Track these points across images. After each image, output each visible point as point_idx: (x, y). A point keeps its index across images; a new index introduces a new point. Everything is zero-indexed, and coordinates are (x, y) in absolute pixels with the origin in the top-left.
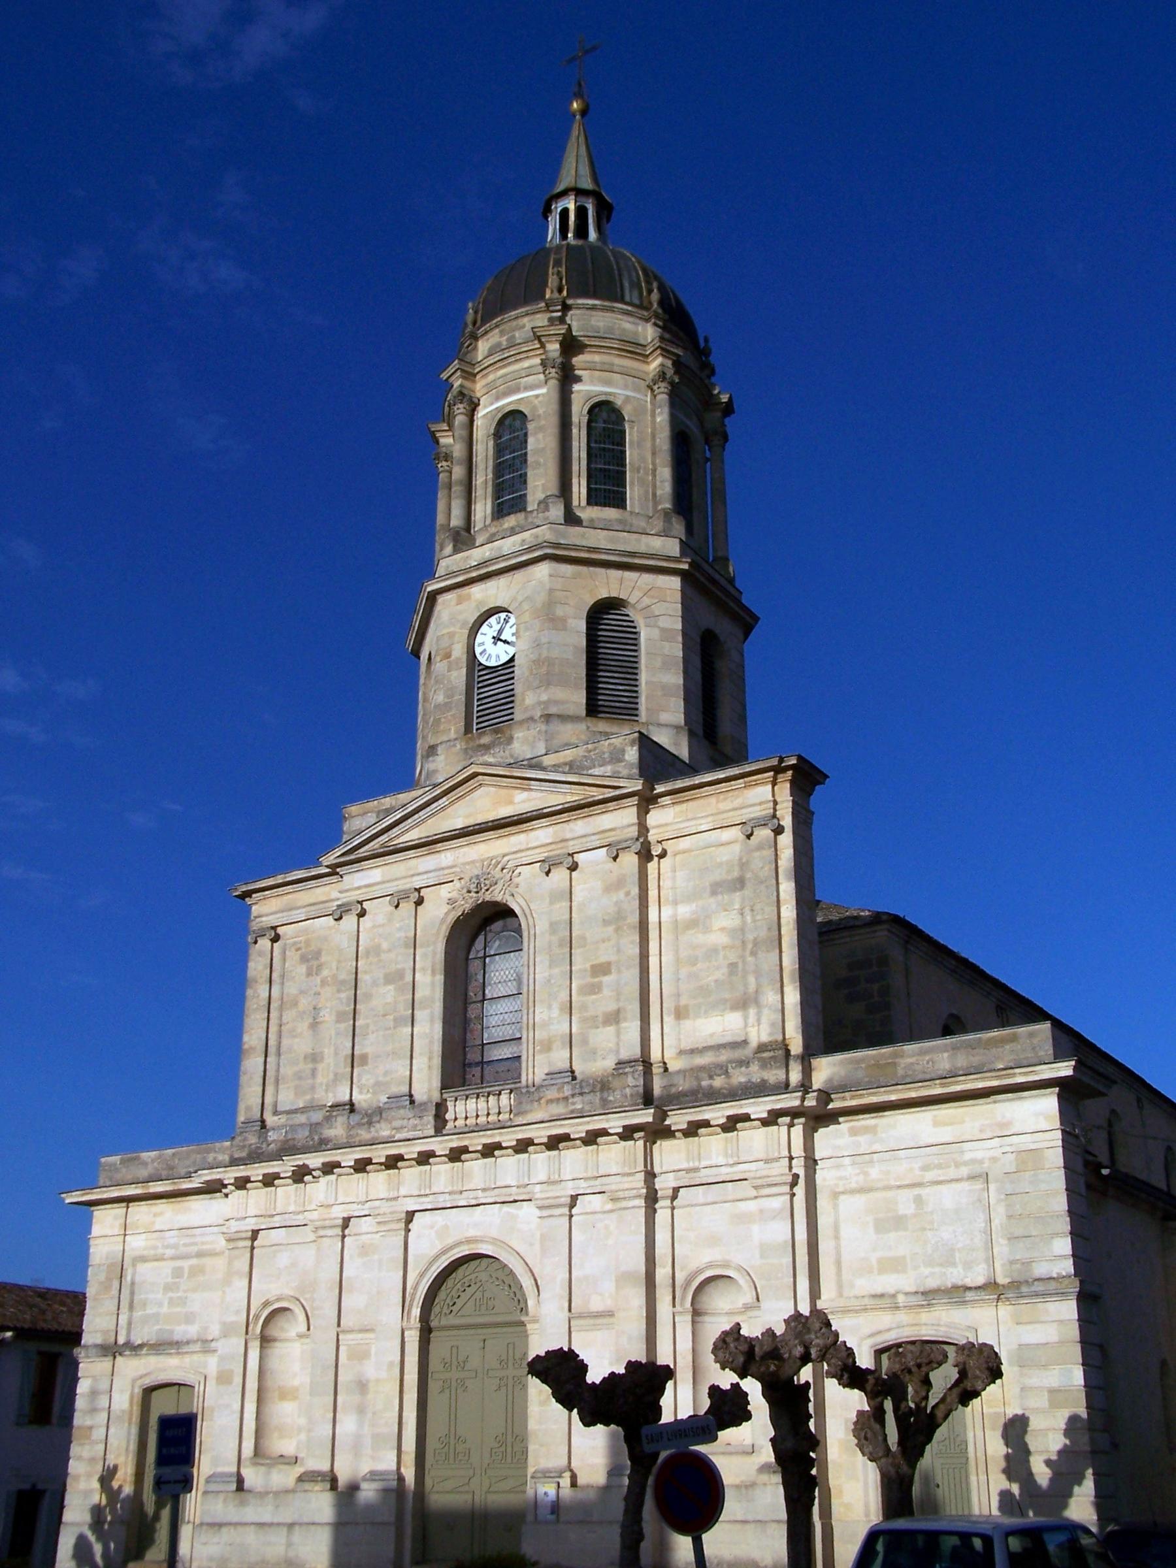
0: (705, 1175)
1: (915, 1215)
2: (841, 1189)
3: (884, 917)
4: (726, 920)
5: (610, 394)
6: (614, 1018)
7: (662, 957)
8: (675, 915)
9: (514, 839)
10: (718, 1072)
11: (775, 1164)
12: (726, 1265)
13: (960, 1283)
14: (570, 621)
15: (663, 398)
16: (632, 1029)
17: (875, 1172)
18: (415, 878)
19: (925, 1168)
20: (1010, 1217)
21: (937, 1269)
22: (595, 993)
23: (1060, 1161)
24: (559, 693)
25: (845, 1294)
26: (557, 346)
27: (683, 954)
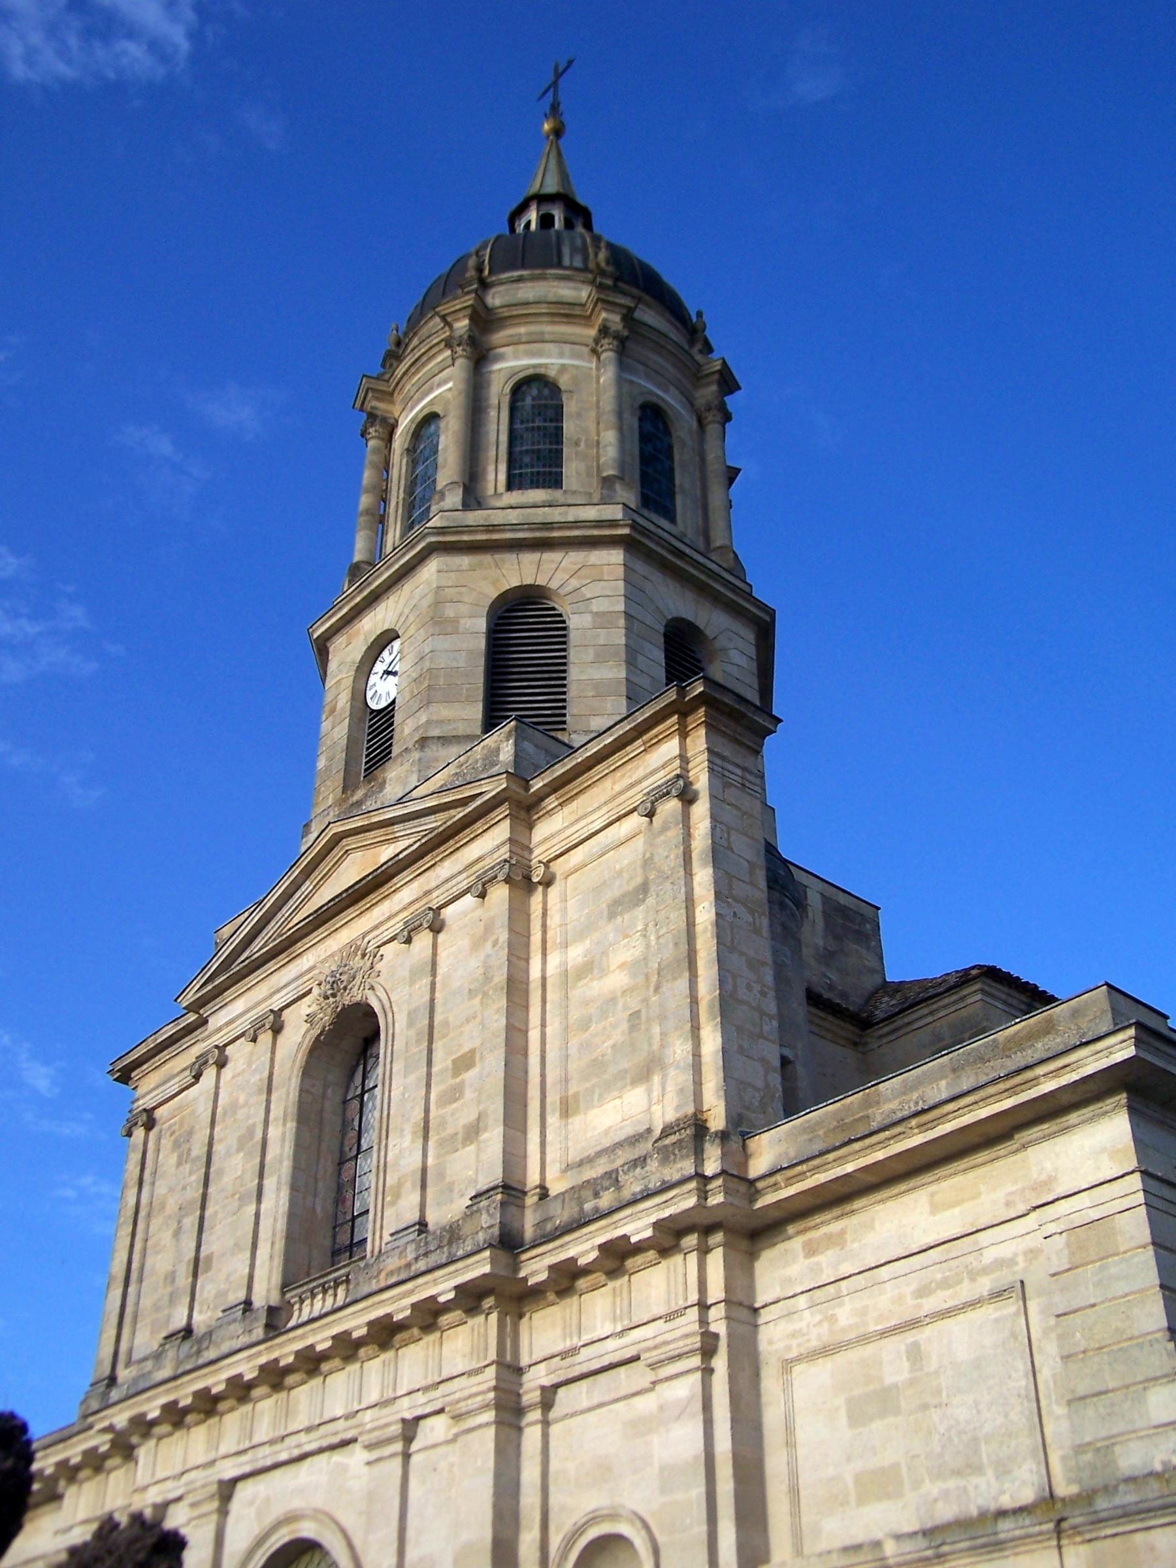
0: (588, 1359)
1: (912, 1382)
2: (793, 1354)
3: (974, 972)
4: (627, 952)
5: (540, 366)
6: (473, 1132)
7: (548, 1030)
8: (565, 963)
10: (606, 1183)
11: (679, 1321)
12: (613, 1516)
13: (993, 1507)
14: (462, 621)
15: (608, 356)
16: (493, 1139)
17: (845, 1314)
19: (923, 1292)
20: (1066, 1358)
21: (952, 1483)
22: (456, 1100)
24: (444, 711)
25: (806, 1551)
26: (466, 322)
27: (575, 1015)
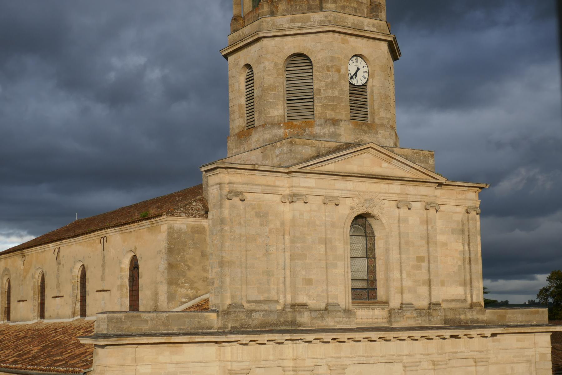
9: (382, 186)
18: (335, 191)
23: (551, 359)
